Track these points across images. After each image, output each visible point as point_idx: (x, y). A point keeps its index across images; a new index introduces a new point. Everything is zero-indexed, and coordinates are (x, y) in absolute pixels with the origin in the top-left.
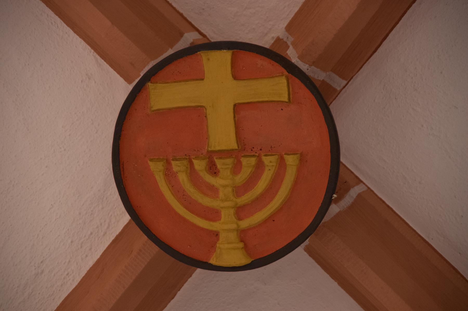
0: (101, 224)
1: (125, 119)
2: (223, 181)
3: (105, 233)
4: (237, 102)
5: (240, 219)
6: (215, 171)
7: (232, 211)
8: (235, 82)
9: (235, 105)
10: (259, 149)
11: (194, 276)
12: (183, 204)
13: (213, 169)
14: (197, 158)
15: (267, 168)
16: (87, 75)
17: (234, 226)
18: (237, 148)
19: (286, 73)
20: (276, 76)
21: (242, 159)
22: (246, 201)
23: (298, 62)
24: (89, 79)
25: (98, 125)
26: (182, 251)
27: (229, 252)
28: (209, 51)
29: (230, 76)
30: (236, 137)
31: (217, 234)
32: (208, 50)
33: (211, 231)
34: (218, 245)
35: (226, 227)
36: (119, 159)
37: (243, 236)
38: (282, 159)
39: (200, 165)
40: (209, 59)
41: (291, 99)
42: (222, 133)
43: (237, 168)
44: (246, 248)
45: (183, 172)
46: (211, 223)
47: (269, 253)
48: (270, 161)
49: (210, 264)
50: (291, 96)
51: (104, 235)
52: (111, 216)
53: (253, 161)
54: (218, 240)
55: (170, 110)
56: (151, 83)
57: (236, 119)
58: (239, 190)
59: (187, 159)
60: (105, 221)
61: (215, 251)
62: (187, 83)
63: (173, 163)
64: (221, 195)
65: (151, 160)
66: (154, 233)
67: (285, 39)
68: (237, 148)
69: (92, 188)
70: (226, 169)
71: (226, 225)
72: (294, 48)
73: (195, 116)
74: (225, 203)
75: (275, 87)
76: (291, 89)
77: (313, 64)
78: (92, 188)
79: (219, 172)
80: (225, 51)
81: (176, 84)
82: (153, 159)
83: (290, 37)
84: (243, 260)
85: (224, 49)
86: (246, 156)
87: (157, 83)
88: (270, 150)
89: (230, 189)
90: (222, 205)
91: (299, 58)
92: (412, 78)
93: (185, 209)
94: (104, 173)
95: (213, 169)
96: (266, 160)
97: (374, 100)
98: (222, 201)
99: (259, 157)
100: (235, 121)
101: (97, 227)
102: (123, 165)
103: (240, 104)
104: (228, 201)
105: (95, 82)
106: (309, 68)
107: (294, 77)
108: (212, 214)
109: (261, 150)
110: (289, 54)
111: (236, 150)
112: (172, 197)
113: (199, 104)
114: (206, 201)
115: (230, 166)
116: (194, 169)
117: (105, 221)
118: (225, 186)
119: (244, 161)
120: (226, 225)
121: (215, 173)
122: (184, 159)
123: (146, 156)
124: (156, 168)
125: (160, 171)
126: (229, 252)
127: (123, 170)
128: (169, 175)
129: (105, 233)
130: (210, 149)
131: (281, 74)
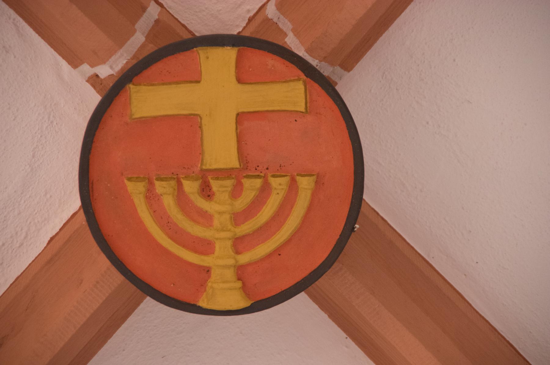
0: (17, 233)
1: (97, 128)
2: (220, 207)
3: (22, 244)
4: (241, 111)
5: (238, 252)
6: (209, 193)
7: (229, 243)
8: (240, 86)
9: (238, 115)
10: (265, 168)
11: (145, 301)
12: (167, 234)
13: (206, 192)
14: (187, 178)
15: (274, 192)
16: (4, 47)
17: (231, 262)
18: (238, 166)
19: (303, 77)
20: (291, 81)
21: (244, 181)
22: (248, 231)
23: (305, 56)
24: (7, 52)
25: (17, 110)
26: (164, 290)
27: (224, 292)
28: (209, 48)
29: (234, 79)
30: (238, 152)
31: (208, 270)
32: (207, 46)
33: (200, 267)
34: (210, 284)
35: (221, 262)
36: (88, 178)
37: (241, 272)
38: (293, 181)
39: (191, 187)
40: (208, 58)
41: (308, 108)
42: (220, 149)
43: (237, 191)
44: (245, 289)
45: (169, 194)
46: (203, 257)
47: (273, 294)
48: (279, 184)
49: (199, 307)
50: (308, 105)
51: (20, 247)
52: (30, 223)
53: (258, 183)
54: (209, 277)
55: (156, 119)
56: (133, 84)
57: (238, 131)
58: (238, 218)
59: (174, 179)
60: (22, 230)
61: (205, 291)
62: (179, 85)
63: (157, 183)
64: (216, 223)
65: (130, 179)
66: (130, 269)
67: (275, 20)
68: (238, 166)
69: (6, 188)
70: (223, 191)
71: (221, 261)
72: (295, 35)
73: (189, 126)
74: (221, 234)
75: (292, 94)
76: (308, 97)
77: (325, 59)
78: (6, 188)
79: (214, 194)
80: (229, 48)
81: (165, 86)
82: (131, 178)
83: (282, 17)
84: (243, 304)
85: (228, 45)
86: (248, 177)
87: (140, 85)
88: (279, 168)
89: (227, 216)
90: (217, 235)
91: (307, 52)
92: (418, 65)
93: (170, 240)
94: (23, 170)
95: (206, 192)
96: (275, 182)
97: (371, 90)
98: (217, 230)
99: (265, 177)
100: (237, 133)
101: (11, 237)
102: (92, 183)
103: (243, 113)
104: (224, 231)
105: (15, 57)
106: (319, 65)
107: (312, 82)
108: (205, 247)
109: (267, 169)
110: (288, 43)
111: (237, 168)
112: (154, 225)
113: (193, 112)
114: (197, 230)
115: (229, 189)
116: (183, 192)
117: (22, 230)
118: (221, 213)
119: (247, 183)
120: (221, 261)
121: (209, 196)
122: (171, 178)
123: (122, 174)
124: (136, 190)
125: (140, 194)
126: (224, 292)
127: (93, 191)
128: (151, 197)
129: (22, 244)
130: (204, 167)
131: (296, 78)
